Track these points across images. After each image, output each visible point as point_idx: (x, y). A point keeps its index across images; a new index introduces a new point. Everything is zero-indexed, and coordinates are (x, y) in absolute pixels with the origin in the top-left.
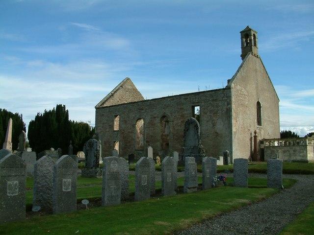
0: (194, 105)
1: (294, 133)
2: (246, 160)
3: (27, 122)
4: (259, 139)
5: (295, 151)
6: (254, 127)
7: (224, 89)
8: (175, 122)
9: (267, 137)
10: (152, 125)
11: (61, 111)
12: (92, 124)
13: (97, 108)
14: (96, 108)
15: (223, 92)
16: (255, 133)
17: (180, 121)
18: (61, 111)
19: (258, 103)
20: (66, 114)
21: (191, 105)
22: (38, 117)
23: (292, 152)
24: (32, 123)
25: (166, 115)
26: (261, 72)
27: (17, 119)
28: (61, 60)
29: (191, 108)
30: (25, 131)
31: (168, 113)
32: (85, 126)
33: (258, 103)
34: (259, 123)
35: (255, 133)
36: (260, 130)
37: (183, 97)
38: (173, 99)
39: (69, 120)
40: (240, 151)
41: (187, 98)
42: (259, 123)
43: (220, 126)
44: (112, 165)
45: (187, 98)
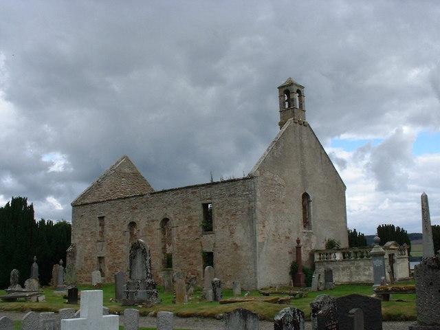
1: (398, 228)
2: (374, 236)
5: (358, 268)
6: (298, 232)
7: (244, 179)
8: (180, 228)
10: (150, 232)
12: (70, 221)
13: (74, 205)
16: (298, 241)
19: (305, 196)
20: (30, 211)
21: (201, 202)
23: (353, 269)
26: (311, 147)
31: (171, 216)
33: (305, 196)
34: (306, 222)
35: (298, 241)
36: (309, 235)
37: (190, 190)
39: (37, 219)
40: (270, 272)
42: (306, 222)
43: (240, 235)
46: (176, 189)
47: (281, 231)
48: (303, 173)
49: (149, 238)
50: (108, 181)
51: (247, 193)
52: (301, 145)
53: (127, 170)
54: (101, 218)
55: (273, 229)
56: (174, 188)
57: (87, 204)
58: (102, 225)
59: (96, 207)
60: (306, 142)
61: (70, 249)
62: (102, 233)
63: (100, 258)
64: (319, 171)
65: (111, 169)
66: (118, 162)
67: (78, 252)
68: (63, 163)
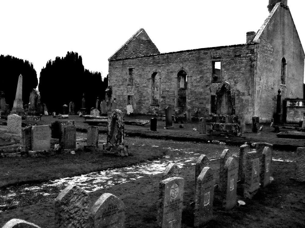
0: (214, 60)
3: (38, 68)
4: (282, 98)
8: (194, 78)
9: (290, 96)
11: (73, 60)
14: (109, 60)
15: (247, 47)
16: (279, 92)
17: (199, 77)
18: (73, 60)
19: (284, 60)
22: (49, 64)
24: (43, 71)
25: (183, 70)
27: (26, 68)
28: (132, 118)
29: (211, 64)
30: (280, 159)
31: (186, 69)
32: (98, 75)
33: (284, 60)
37: (202, 51)
38: (192, 54)
41: (207, 53)
42: (283, 80)
44: (171, 190)
45: (207, 53)
46: (191, 50)
47: (269, 84)
48: (283, 43)
49: (168, 84)
50: (132, 45)
51: (250, 55)
52: (283, 23)
53: (144, 38)
54: (131, 70)
55: (265, 82)
56: (190, 49)
57: (283, 49)
58: (130, 74)
59: (127, 62)
60: (286, 21)
61: (107, 90)
62: (131, 79)
63: (129, 97)
64: (292, 43)
65: (134, 38)
66: (138, 33)
67: (113, 92)
68: (283, 8)
